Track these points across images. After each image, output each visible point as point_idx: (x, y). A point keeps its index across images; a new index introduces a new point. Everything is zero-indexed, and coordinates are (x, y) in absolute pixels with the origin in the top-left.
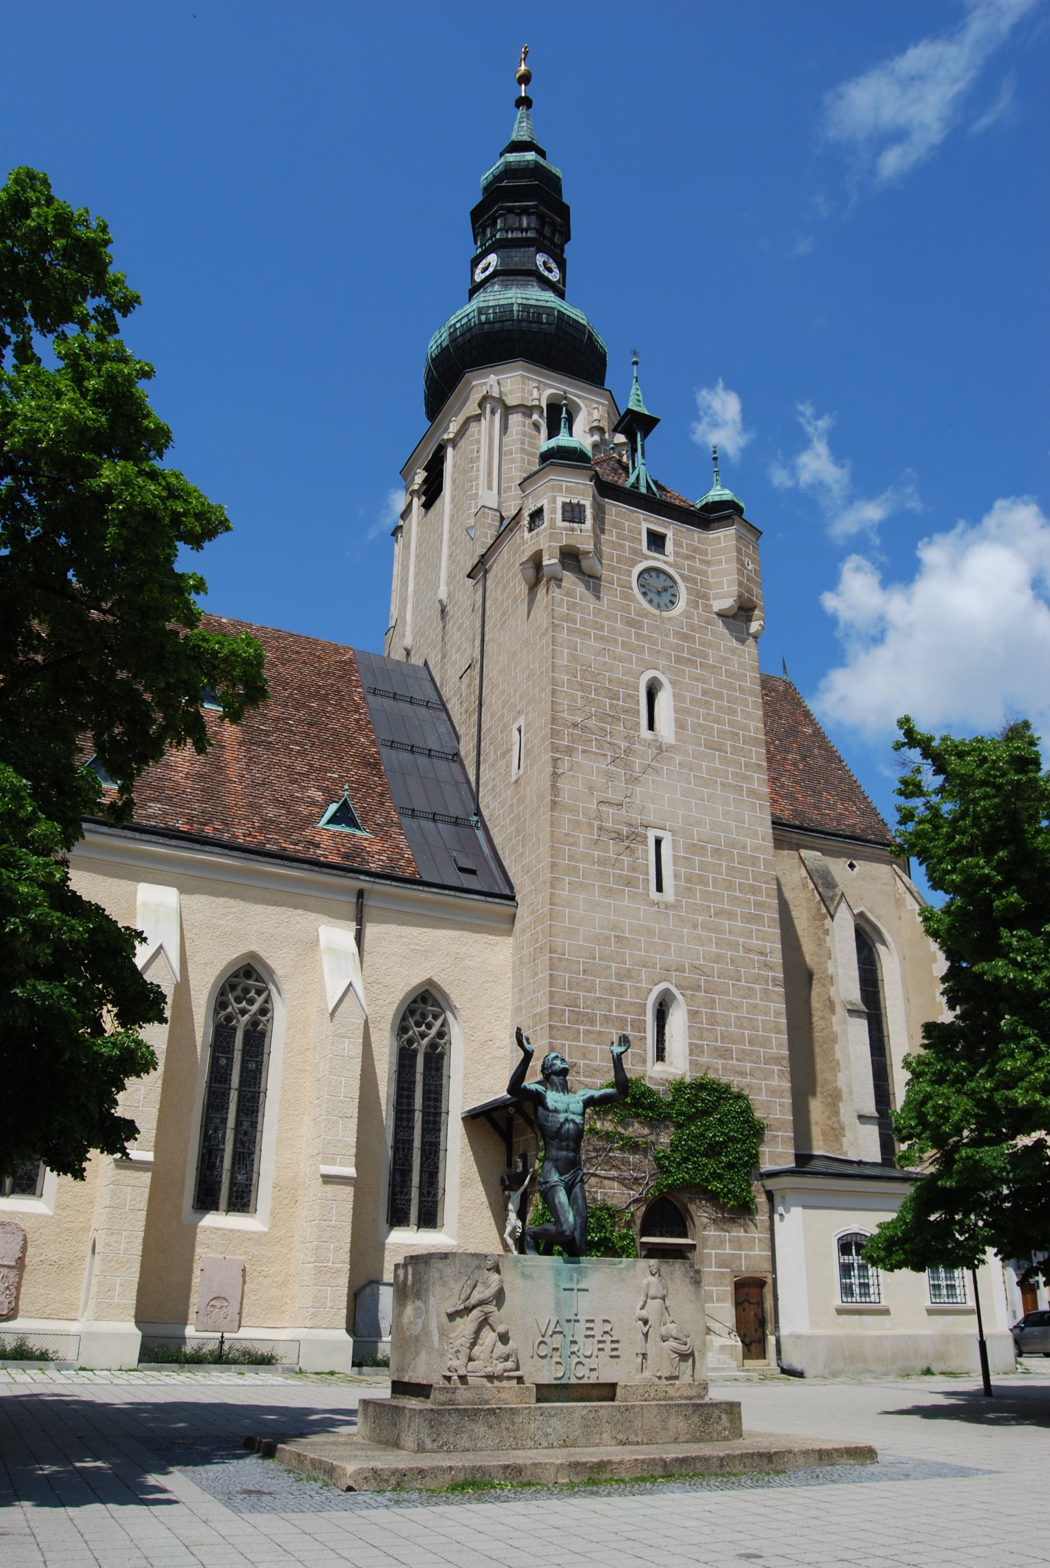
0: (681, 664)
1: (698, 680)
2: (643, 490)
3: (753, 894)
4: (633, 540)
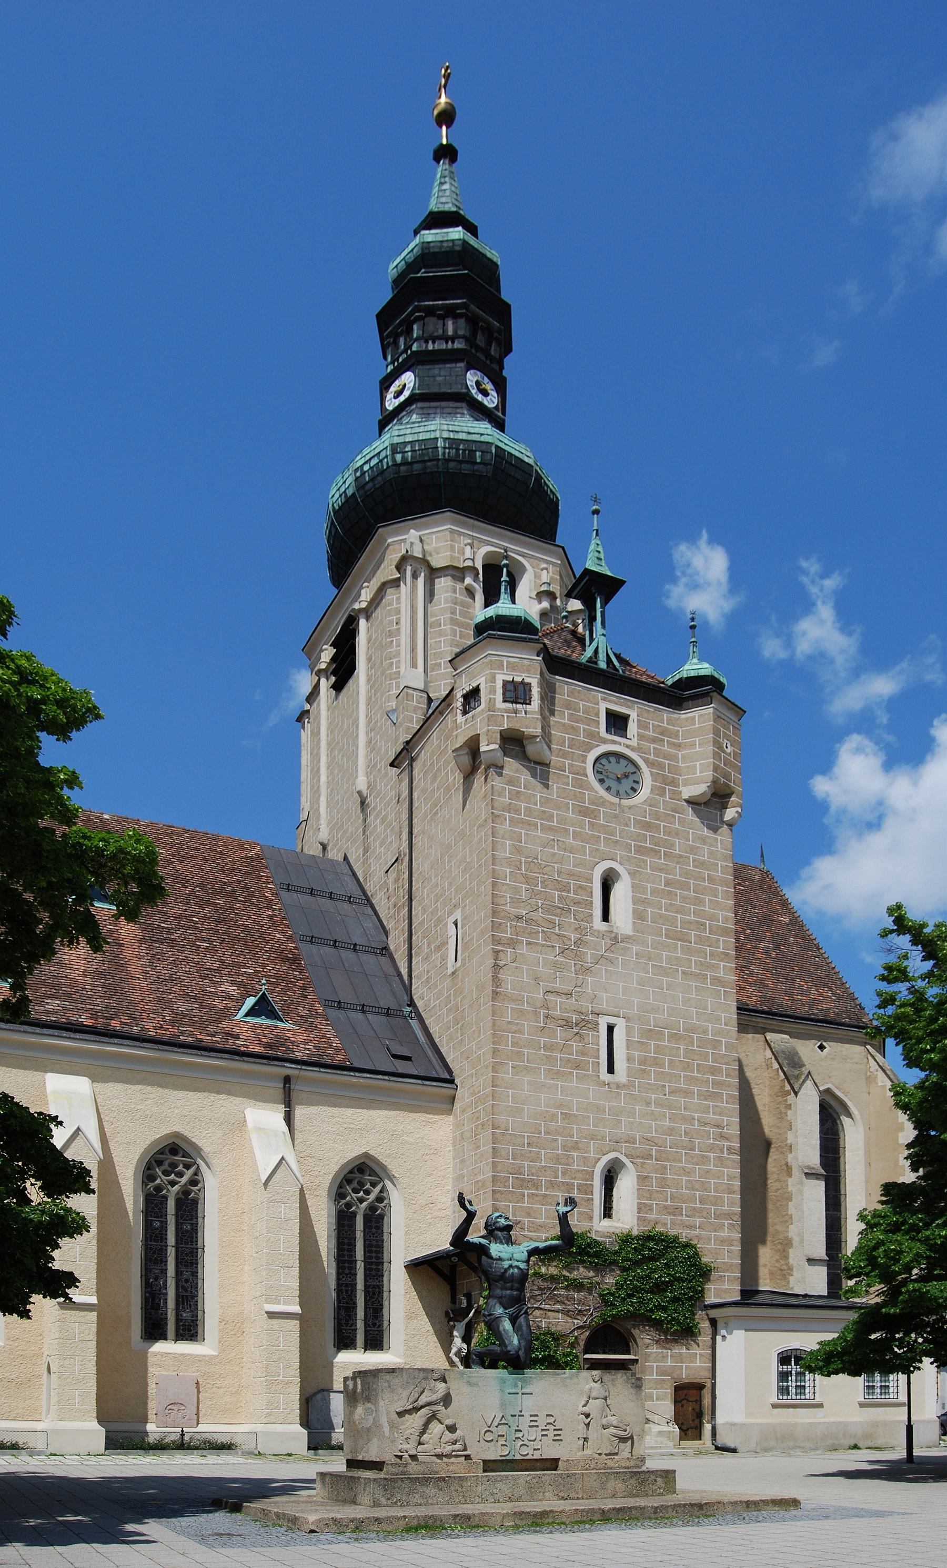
0: (642, 854)
1: (661, 870)
2: (603, 665)
3: (712, 1074)
4: (588, 721)
